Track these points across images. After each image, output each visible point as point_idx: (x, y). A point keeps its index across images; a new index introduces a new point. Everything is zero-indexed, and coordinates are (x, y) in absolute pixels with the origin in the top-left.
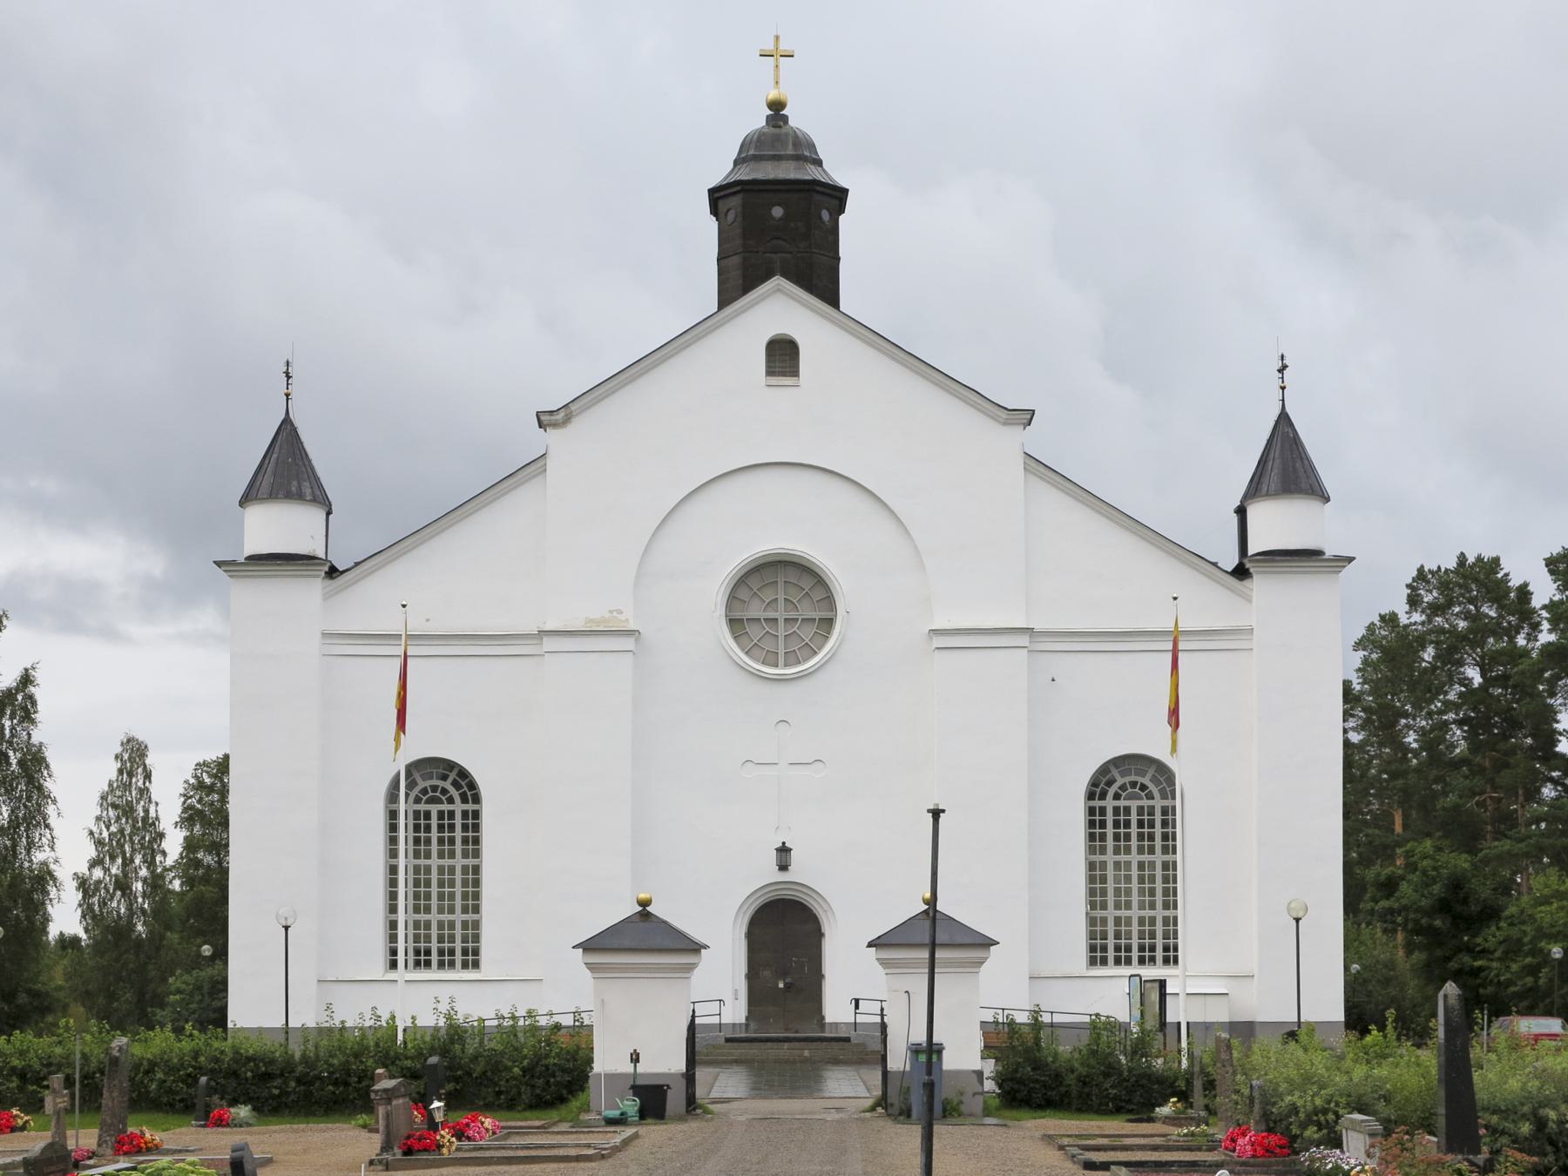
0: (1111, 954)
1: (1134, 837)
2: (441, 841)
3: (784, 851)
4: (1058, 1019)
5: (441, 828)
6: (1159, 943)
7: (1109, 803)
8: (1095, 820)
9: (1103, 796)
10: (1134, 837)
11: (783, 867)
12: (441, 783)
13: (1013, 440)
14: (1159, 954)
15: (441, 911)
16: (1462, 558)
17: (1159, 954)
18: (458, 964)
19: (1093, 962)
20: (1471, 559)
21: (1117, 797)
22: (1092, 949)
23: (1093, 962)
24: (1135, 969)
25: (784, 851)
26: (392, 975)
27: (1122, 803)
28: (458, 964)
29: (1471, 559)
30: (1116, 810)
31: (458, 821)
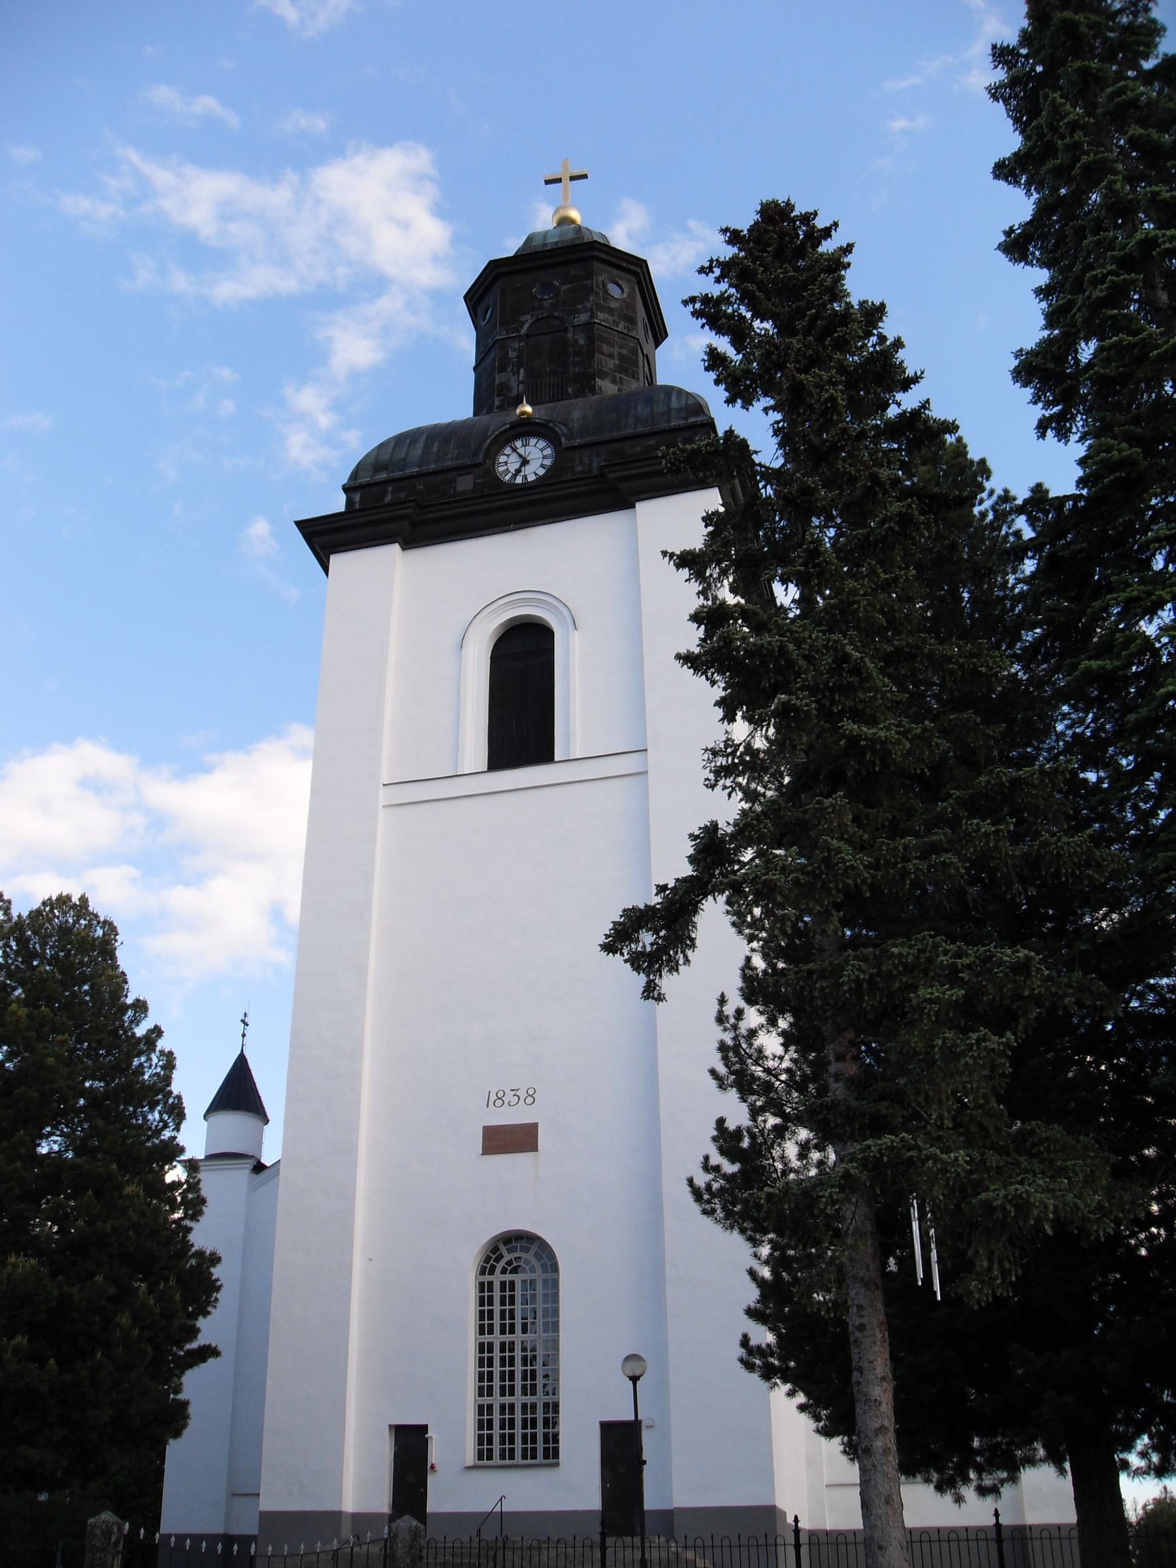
9: (492, 1272)
12: (502, 1263)
18: (518, 1453)
21: (504, 1271)
27: (508, 1277)
28: (518, 1453)
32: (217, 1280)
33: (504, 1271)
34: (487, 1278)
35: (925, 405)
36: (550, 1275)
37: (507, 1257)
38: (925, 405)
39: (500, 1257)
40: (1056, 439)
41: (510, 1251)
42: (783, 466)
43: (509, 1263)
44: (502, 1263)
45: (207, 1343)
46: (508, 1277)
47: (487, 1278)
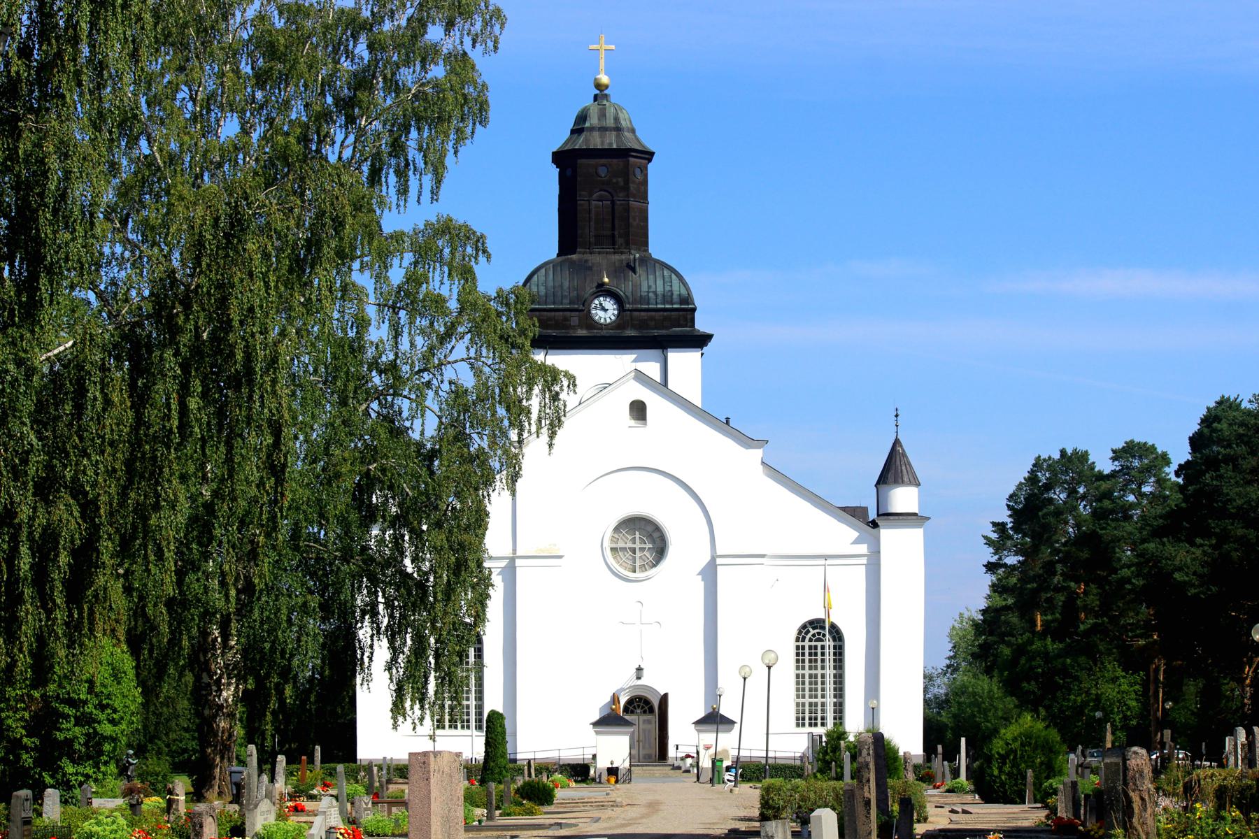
0: (807, 721)
1: (807, 661)
2: (810, 661)
3: (639, 669)
4: (778, 755)
5: (810, 654)
6: (819, 715)
7: (807, 643)
8: (800, 651)
9: (803, 640)
10: (807, 661)
11: (639, 678)
12: (809, 635)
13: (757, 454)
14: (819, 721)
15: (810, 697)
16: (1063, 452)
17: (819, 721)
18: (807, 724)
19: (798, 725)
20: (1069, 451)
21: (810, 640)
22: (798, 719)
23: (798, 725)
24: (807, 729)
25: (639, 669)
26: (801, 729)
27: (813, 643)
28: (807, 724)
29: (1069, 451)
30: (810, 647)
31: (807, 651)
32: (1063, 452)
33: (810, 640)
34: (800, 644)
35: (856, 542)
36: (838, 643)
37: (812, 632)
38: (856, 542)
39: (808, 632)
40: (1226, 397)
41: (814, 629)
42: (52, 786)
43: (814, 635)
44: (809, 635)
45: (1204, 412)
46: (813, 643)
47: (800, 644)
